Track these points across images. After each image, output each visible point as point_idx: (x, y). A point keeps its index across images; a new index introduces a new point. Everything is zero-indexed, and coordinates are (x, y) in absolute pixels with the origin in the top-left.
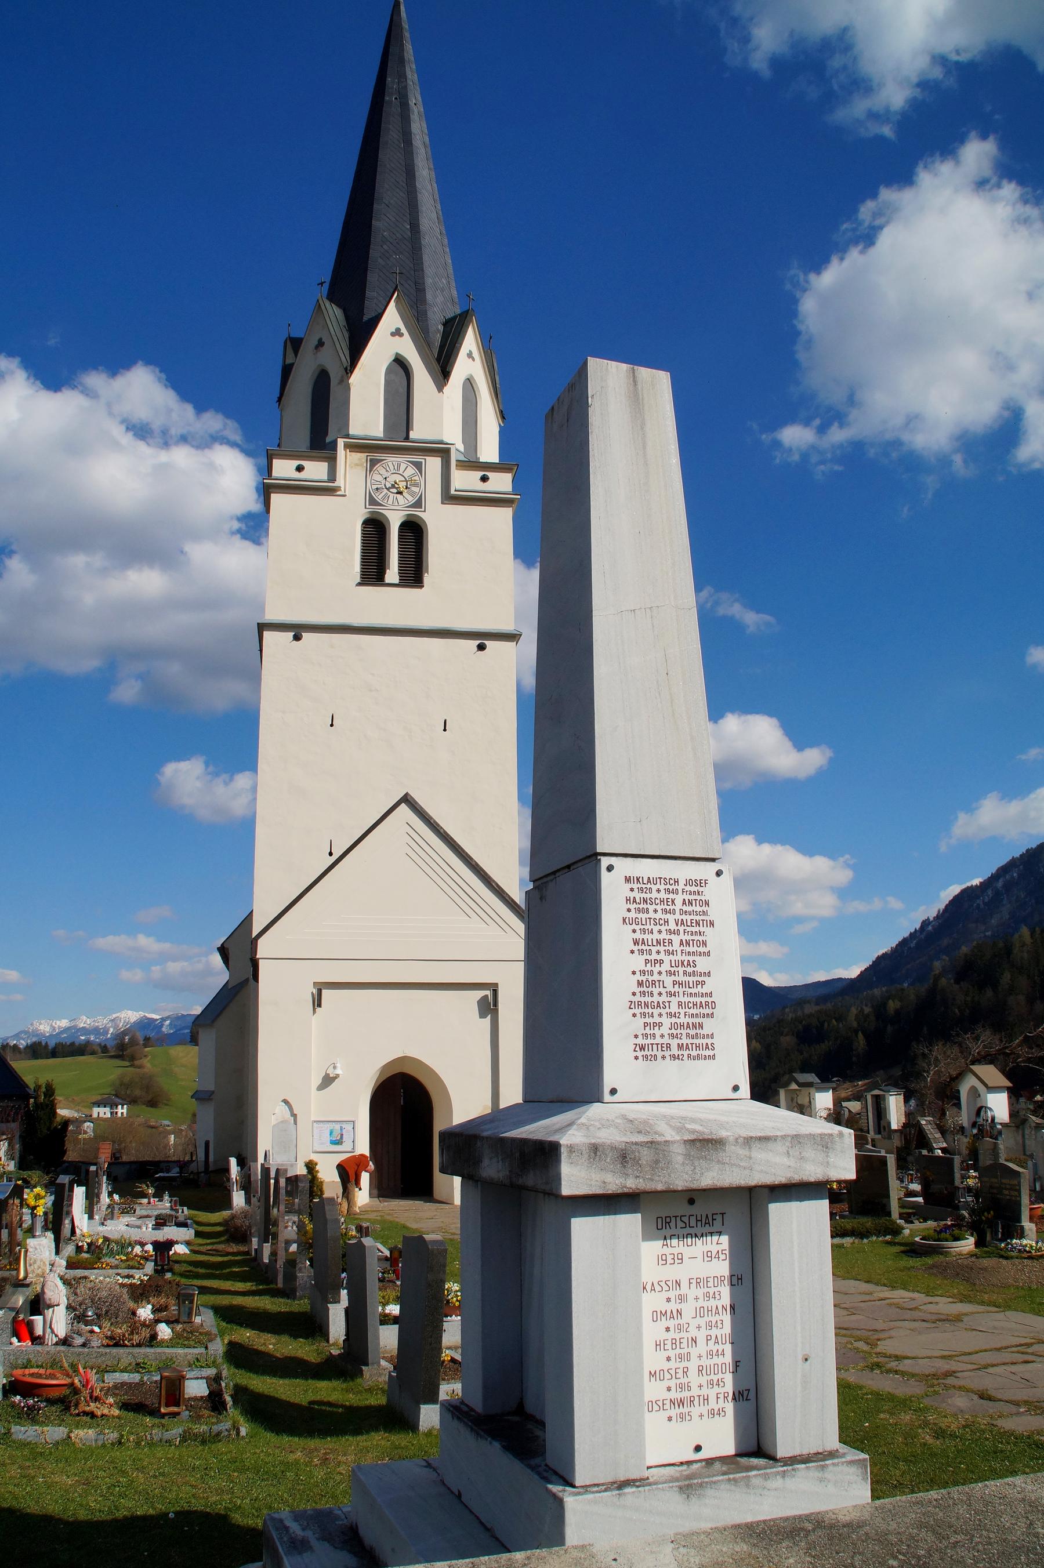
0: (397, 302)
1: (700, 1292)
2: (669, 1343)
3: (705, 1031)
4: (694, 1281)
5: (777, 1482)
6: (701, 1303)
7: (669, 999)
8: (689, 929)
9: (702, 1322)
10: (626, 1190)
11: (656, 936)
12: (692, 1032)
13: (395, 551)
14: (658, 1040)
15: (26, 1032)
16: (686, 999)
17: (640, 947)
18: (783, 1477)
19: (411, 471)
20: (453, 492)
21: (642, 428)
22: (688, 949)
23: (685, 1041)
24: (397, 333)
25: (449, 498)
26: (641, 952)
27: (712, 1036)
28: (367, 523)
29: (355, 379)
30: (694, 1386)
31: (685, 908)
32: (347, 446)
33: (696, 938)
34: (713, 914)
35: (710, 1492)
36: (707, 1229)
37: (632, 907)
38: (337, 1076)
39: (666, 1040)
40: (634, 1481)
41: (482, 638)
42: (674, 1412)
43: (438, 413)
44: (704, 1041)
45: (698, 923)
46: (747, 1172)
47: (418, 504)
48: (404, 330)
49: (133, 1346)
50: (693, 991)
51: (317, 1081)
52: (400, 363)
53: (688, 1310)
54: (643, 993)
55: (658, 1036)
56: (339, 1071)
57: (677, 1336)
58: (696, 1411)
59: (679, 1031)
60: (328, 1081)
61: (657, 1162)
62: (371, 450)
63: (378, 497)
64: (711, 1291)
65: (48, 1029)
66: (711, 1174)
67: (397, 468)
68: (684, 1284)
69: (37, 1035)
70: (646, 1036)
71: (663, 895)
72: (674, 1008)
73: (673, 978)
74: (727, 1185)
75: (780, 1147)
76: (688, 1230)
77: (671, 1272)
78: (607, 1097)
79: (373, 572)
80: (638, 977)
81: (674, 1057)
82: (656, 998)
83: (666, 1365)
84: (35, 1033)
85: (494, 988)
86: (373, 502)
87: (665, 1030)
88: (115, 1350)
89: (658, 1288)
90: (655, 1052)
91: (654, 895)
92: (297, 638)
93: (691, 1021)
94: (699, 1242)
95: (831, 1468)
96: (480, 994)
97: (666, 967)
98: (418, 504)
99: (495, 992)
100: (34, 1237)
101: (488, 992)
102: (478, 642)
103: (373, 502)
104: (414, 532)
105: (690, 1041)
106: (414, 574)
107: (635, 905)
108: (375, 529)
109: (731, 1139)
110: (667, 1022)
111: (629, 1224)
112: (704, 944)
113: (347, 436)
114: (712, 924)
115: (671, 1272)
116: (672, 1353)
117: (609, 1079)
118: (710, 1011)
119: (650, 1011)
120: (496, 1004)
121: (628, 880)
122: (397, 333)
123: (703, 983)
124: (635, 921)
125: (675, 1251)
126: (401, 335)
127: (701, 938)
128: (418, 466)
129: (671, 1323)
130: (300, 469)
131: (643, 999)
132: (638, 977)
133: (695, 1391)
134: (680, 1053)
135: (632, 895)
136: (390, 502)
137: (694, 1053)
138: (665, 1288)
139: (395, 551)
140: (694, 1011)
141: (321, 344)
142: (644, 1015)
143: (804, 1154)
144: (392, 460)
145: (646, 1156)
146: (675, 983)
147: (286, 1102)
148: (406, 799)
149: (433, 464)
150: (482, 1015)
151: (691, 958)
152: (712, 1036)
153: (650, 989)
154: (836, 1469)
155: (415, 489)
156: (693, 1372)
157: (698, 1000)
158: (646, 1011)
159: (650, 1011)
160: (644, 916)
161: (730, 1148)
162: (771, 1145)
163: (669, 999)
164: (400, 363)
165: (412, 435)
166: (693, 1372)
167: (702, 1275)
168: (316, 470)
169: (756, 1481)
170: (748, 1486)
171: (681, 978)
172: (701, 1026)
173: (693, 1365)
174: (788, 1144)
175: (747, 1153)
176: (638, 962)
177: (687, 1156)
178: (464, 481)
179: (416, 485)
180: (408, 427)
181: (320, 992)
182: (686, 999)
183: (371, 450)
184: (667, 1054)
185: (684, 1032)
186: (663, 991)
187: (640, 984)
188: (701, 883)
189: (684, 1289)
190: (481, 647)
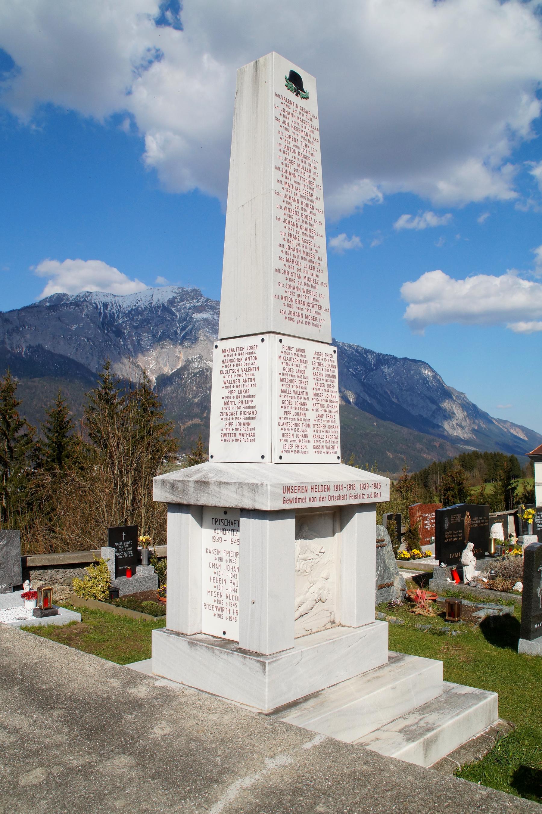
1: (228, 558)
2: (215, 579)
3: (251, 426)
4: (226, 552)
5: (225, 656)
6: (228, 564)
7: (237, 410)
8: (247, 373)
9: (229, 573)
10: (173, 502)
11: (233, 378)
12: (245, 427)
14: (231, 432)
16: (244, 410)
17: (226, 385)
18: (228, 655)
21: (257, 96)
22: (246, 384)
23: (242, 432)
26: (227, 387)
27: (254, 429)
30: (224, 602)
31: (247, 362)
33: (250, 377)
34: (259, 363)
35: (199, 648)
36: (232, 527)
37: (224, 364)
39: (234, 432)
40: (185, 635)
42: (217, 612)
44: (250, 432)
45: (251, 369)
46: (218, 499)
49: (498, 590)
50: (247, 405)
53: (223, 565)
54: (226, 408)
55: (231, 429)
57: (219, 577)
58: (225, 615)
59: (240, 427)
61: (184, 490)
64: (233, 558)
66: (204, 498)
68: (222, 552)
70: (226, 429)
71: (237, 357)
72: (238, 415)
73: (239, 399)
74: (210, 505)
75: (233, 488)
76: (224, 527)
77: (218, 546)
78: (210, 459)
80: (225, 400)
81: (237, 440)
82: (231, 410)
83: (214, 590)
87: (234, 426)
88: (487, 591)
89: (212, 552)
90: (229, 438)
91: (234, 357)
93: (245, 421)
94: (228, 533)
95: (248, 659)
97: (236, 394)
100: (528, 534)
105: (244, 432)
107: (226, 364)
109: (213, 482)
110: (235, 422)
111: (188, 518)
112: (254, 380)
114: (258, 369)
115: (218, 546)
116: (216, 585)
117: (211, 452)
118: (253, 416)
119: (229, 417)
121: (223, 351)
123: (252, 401)
124: (225, 372)
125: (219, 536)
127: (252, 377)
129: (216, 570)
131: (226, 411)
132: (225, 400)
133: (224, 606)
134: (240, 438)
135: (224, 359)
137: (246, 438)
138: (215, 553)
140: (247, 416)
142: (226, 419)
143: (244, 493)
145: (180, 486)
146: (239, 402)
151: (247, 388)
152: (254, 429)
153: (229, 406)
154: (251, 661)
156: (224, 596)
157: (249, 410)
158: (227, 417)
159: (229, 417)
160: (228, 369)
161: (213, 487)
162: (229, 487)
163: (237, 410)
166: (224, 596)
167: (229, 550)
169: (216, 652)
170: (213, 653)
171: (242, 399)
172: (249, 424)
173: (224, 593)
174: (236, 487)
175: (219, 490)
176: (225, 393)
177: (195, 488)
182: (244, 410)
184: (234, 438)
185: (242, 427)
186: (234, 406)
187: (225, 403)
188: (255, 347)
189: (222, 555)
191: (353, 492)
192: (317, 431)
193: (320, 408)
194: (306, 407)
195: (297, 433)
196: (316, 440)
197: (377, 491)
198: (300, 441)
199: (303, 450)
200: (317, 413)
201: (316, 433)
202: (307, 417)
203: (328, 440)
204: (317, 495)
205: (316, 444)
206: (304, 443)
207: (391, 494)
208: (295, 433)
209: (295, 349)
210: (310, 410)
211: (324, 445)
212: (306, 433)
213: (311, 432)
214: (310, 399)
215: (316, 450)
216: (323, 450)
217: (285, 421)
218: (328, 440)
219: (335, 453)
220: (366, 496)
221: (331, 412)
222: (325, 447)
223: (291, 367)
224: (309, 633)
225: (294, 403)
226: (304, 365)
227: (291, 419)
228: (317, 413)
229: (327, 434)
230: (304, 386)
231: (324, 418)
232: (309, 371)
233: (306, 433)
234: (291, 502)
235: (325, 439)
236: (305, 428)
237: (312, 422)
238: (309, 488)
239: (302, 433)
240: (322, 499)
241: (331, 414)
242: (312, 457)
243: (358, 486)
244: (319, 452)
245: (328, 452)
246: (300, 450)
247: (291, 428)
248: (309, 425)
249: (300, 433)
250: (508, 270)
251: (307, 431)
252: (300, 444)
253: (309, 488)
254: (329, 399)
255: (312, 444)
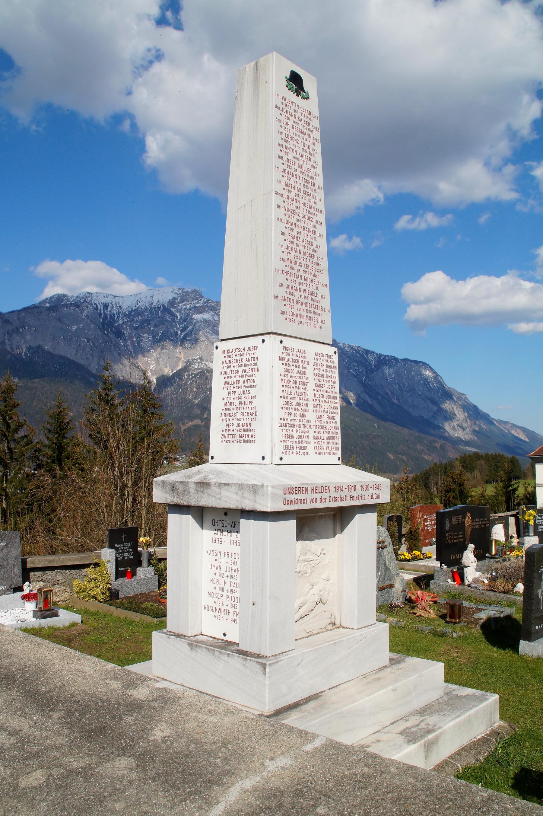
1: (229, 559)
2: (215, 580)
3: (252, 428)
4: (226, 553)
5: (225, 658)
6: (229, 565)
7: (237, 411)
8: (248, 374)
9: (229, 574)
10: (174, 503)
11: (234, 379)
12: (246, 428)
14: (232, 433)
16: (244, 411)
17: (227, 386)
18: (228, 656)
21: (258, 96)
22: (247, 385)
23: (243, 433)
26: (227, 388)
27: (254, 430)
30: (225, 604)
31: (247, 363)
33: (250, 378)
34: (259, 364)
35: (199, 650)
36: (232, 529)
37: (225, 365)
39: (235, 433)
40: (185, 636)
42: (217, 614)
44: (251, 433)
45: (252, 370)
46: (219, 500)
49: (499, 592)
50: (247, 406)
53: (224, 566)
54: (227, 409)
55: (231, 430)
57: (219, 579)
58: (226, 616)
59: (240, 428)
61: (184, 491)
64: (233, 560)
66: (204, 500)
68: (222, 554)
70: (226, 430)
71: (238, 358)
72: (239, 416)
73: (240, 400)
74: (210, 506)
75: (233, 489)
76: (224, 528)
77: (218, 547)
78: (210, 460)
80: (225, 401)
81: (238, 441)
82: (232, 411)
83: (215, 591)
87: (234, 427)
88: (488, 593)
89: (212, 554)
90: (230, 439)
91: (234, 358)
93: (246, 422)
94: (229, 535)
95: (248, 661)
97: (237, 395)
105: (245, 433)
107: (226, 365)
109: (213, 483)
110: (235, 423)
111: (188, 520)
112: (254, 381)
114: (258, 369)
115: (218, 547)
116: (217, 586)
117: (211, 453)
118: (254, 417)
119: (229, 418)
121: (224, 352)
123: (252, 402)
124: (226, 373)
125: (220, 537)
127: (253, 378)
129: (217, 572)
131: (226, 412)
132: (225, 401)
133: (225, 607)
134: (240, 439)
135: (225, 359)
137: (246, 439)
138: (215, 554)
140: (247, 417)
142: (226, 420)
143: (244, 495)
145: (180, 487)
146: (240, 403)
151: (248, 389)
152: (254, 430)
153: (229, 407)
154: (251, 663)
156: (225, 597)
157: (249, 411)
158: (227, 418)
159: (229, 418)
160: (229, 370)
161: (213, 489)
162: (230, 488)
163: (237, 411)
166: (225, 597)
167: (230, 552)
169: (217, 653)
170: (213, 654)
171: (243, 400)
172: (250, 425)
173: (225, 594)
174: (237, 488)
175: (219, 491)
176: (225, 394)
177: (196, 489)
182: (244, 411)
184: (234, 439)
185: (242, 428)
186: (235, 407)
187: (226, 404)
188: (255, 348)
189: (222, 556)
191: (354, 494)
192: (318, 432)
193: (321, 409)
194: (306, 408)
195: (298, 434)
196: (316, 441)
197: (378, 492)
198: (300, 442)
199: (304, 451)
200: (318, 414)
201: (316, 434)
202: (308, 418)
203: (328, 441)
204: (318, 496)
205: (316, 445)
206: (305, 445)
207: (392, 495)
208: (296, 434)
209: (295, 350)
210: (311, 411)
211: (325, 446)
212: (306, 434)
213: (311, 434)
214: (311, 400)
215: (317, 451)
216: (323, 451)
217: (286, 422)
218: (328, 441)
219: (336, 454)
220: (366, 497)
221: (331, 413)
222: (325, 448)
223: (291, 368)
224: (309, 634)
225: (294, 404)
226: (305, 366)
227: (292, 420)
228: (318, 414)
229: (328, 435)
230: (304, 387)
231: (325, 419)
232: (310, 372)
233: (306, 434)
234: (291, 503)
235: (325, 441)
236: (306, 430)
237: (312, 423)
238: (310, 489)
239: (303, 434)
240: (323, 500)
241: (332, 415)
242: (313, 458)
243: (358, 487)
244: (320, 453)
245: (329, 454)
246: (301, 451)
247: (291, 429)
248: (310, 426)
249: (300, 434)
250: (509, 271)
251: (307, 432)
252: (300, 445)
253: (310, 489)
254: (329, 400)
255: (313, 445)
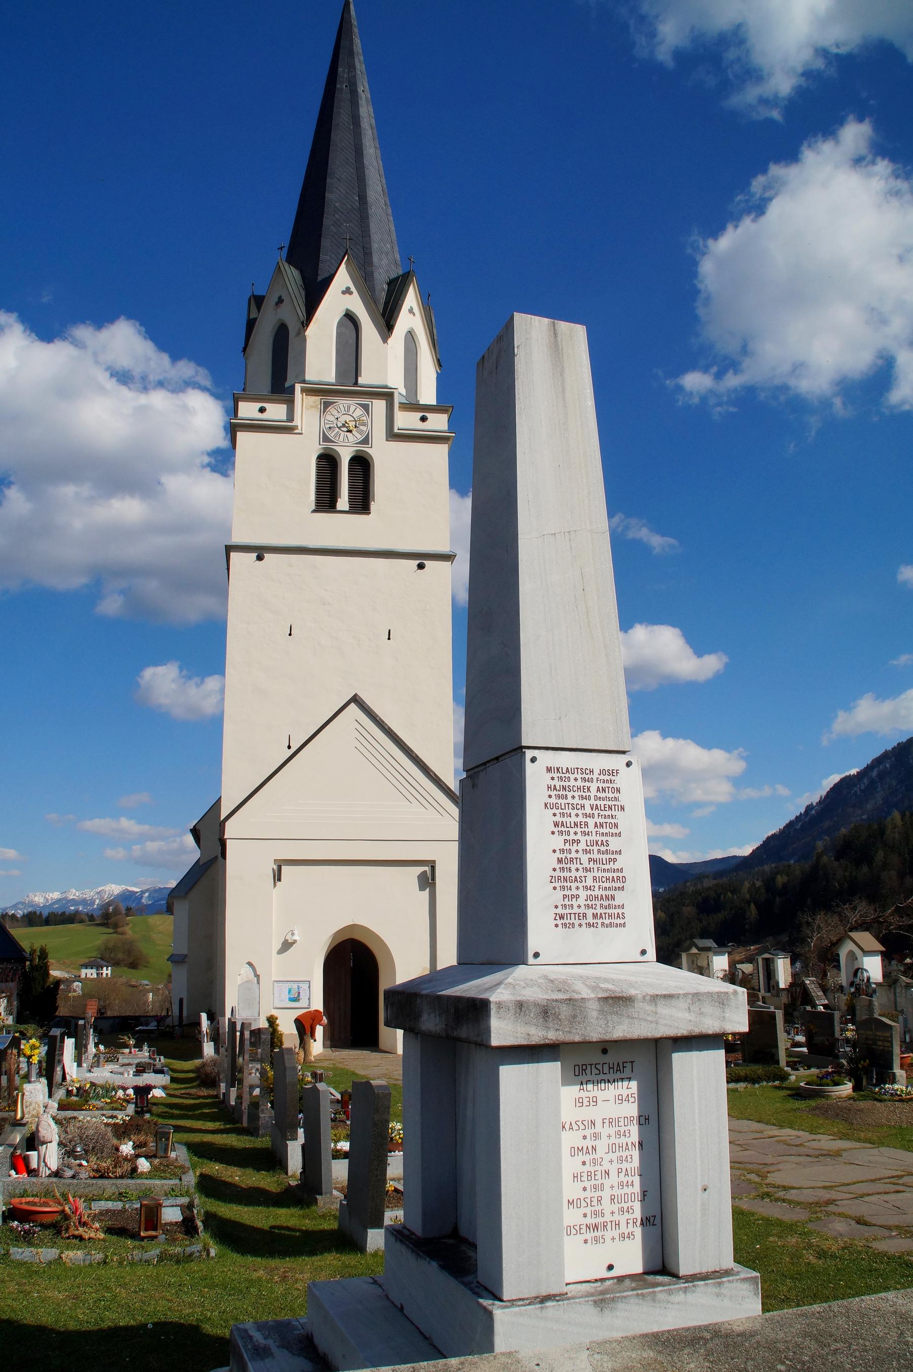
0: (347, 264)
1: (612, 1131)
2: (585, 1175)
3: (617, 902)
4: (607, 1121)
5: (680, 1297)
6: (613, 1140)
7: (585, 874)
8: (602, 813)
9: (614, 1157)
10: (547, 1041)
11: (574, 819)
12: (606, 903)
13: (345, 482)
14: (576, 910)
15: (23, 903)
16: (600, 874)
17: (560, 829)
18: (685, 1292)
19: (359, 412)
20: (396, 431)
21: (562, 375)
22: (601, 830)
23: (599, 911)
24: (347, 291)
25: (393, 435)
26: (561, 833)
27: (623, 906)
28: (321, 457)
29: (310, 332)
30: (607, 1212)
31: (599, 795)
32: (303, 390)
33: (608, 821)
34: (623, 799)
35: (620, 1305)
36: (619, 1075)
37: (553, 793)
38: (295, 942)
39: (582, 910)
40: (555, 1296)
41: (421, 559)
42: (589, 1236)
43: (383, 362)
44: (616, 911)
45: (610, 808)
46: (653, 1025)
47: (366, 441)
48: (353, 289)
49: (116, 1177)
50: (606, 867)
51: (277, 945)
52: (350, 317)
53: (602, 1146)
54: (562, 869)
55: (575, 907)
56: (296, 937)
57: (592, 1169)
58: (608, 1234)
59: (594, 902)
60: (287, 946)
61: (575, 1017)
62: (325, 393)
63: (331, 435)
64: (622, 1129)
65: (42, 900)
66: (622, 1027)
67: (347, 409)
68: (599, 1124)
69: (33, 906)
70: (565, 906)
71: (580, 783)
72: (590, 882)
73: (589, 856)
74: (636, 1037)
75: (682, 1004)
76: (602, 1076)
77: (587, 1113)
78: (531, 960)
79: (326, 500)
80: (558, 855)
81: (589, 925)
82: (574, 874)
83: (583, 1195)
84: (31, 904)
85: (432, 865)
86: (326, 439)
87: (582, 901)
88: (100, 1182)
89: (575, 1127)
90: (573, 920)
91: (572, 783)
92: (260, 558)
93: (604, 893)
94: (611, 1087)
95: (727, 1284)
96: (420, 870)
97: (582, 846)
98: (366, 441)
99: (433, 868)
101: (426, 868)
102: (418, 562)
103: (326, 439)
104: (362, 465)
105: (603, 911)
106: (362, 502)
107: (555, 792)
108: (328, 463)
109: (639, 996)
110: (583, 894)
111: (550, 1071)
112: (616, 826)
113: (304, 382)
114: (623, 808)
115: (587, 1113)
116: (587, 1184)
117: (533, 944)
118: (620, 885)
119: (569, 884)
120: (433, 878)
121: (549, 770)
122: (347, 291)
123: (615, 860)
124: (555, 806)
125: (591, 1095)
126: (351, 293)
127: (613, 821)
128: (366, 407)
129: (587, 1158)
130: (262, 410)
131: (562, 874)
132: (558, 855)
133: (608, 1217)
134: (595, 921)
135: (553, 783)
136: (341, 439)
137: (607, 921)
138: (582, 1127)
139: (345, 482)
140: (607, 885)
141: (280, 301)
142: (563, 888)
143: (703, 1010)
144: (342, 403)
145: (565, 1011)
146: (590, 860)
147: (250, 964)
148: (355, 700)
149: (379, 406)
150: (422, 888)
151: (604, 839)
152: (623, 906)
153: (568, 866)
154: (731, 1285)
155: (363, 428)
156: (606, 1200)
157: (610, 875)
158: (565, 884)
159: (569, 884)
160: (563, 801)
161: (638, 1005)
162: (674, 1002)
163: (585, 874)
164: (350, 317)
165: (361, 381)
166: (606, 1200)
167: (614, 1116)
168: (276, 412)
169: (661, 1296)
170: (654, 1300)
171: (596, 856)
172: (613, 898)
173: (606, 1195)
174: (689, 1001)
175: (653, 1009)
176: (558, 842)
177: (601, 1011)
178: (406, 420)
179: (364, 424)
180: (357, 373)
181: (280, 868)
182: (600, 874)
183: (325, 393)
184: (583, 922)
185: (598, 903)
186: (580, 867)
187: (560, 861)
188: (613, 772)
189: (598, 1127)
190: (421, 567)
209: (596, 772)
